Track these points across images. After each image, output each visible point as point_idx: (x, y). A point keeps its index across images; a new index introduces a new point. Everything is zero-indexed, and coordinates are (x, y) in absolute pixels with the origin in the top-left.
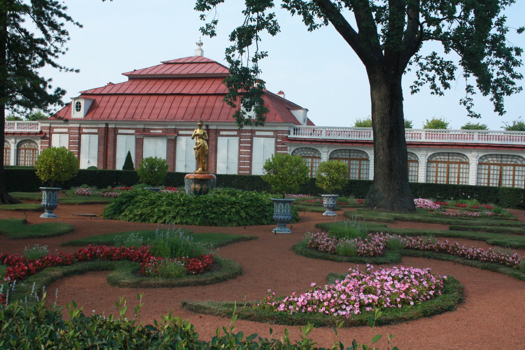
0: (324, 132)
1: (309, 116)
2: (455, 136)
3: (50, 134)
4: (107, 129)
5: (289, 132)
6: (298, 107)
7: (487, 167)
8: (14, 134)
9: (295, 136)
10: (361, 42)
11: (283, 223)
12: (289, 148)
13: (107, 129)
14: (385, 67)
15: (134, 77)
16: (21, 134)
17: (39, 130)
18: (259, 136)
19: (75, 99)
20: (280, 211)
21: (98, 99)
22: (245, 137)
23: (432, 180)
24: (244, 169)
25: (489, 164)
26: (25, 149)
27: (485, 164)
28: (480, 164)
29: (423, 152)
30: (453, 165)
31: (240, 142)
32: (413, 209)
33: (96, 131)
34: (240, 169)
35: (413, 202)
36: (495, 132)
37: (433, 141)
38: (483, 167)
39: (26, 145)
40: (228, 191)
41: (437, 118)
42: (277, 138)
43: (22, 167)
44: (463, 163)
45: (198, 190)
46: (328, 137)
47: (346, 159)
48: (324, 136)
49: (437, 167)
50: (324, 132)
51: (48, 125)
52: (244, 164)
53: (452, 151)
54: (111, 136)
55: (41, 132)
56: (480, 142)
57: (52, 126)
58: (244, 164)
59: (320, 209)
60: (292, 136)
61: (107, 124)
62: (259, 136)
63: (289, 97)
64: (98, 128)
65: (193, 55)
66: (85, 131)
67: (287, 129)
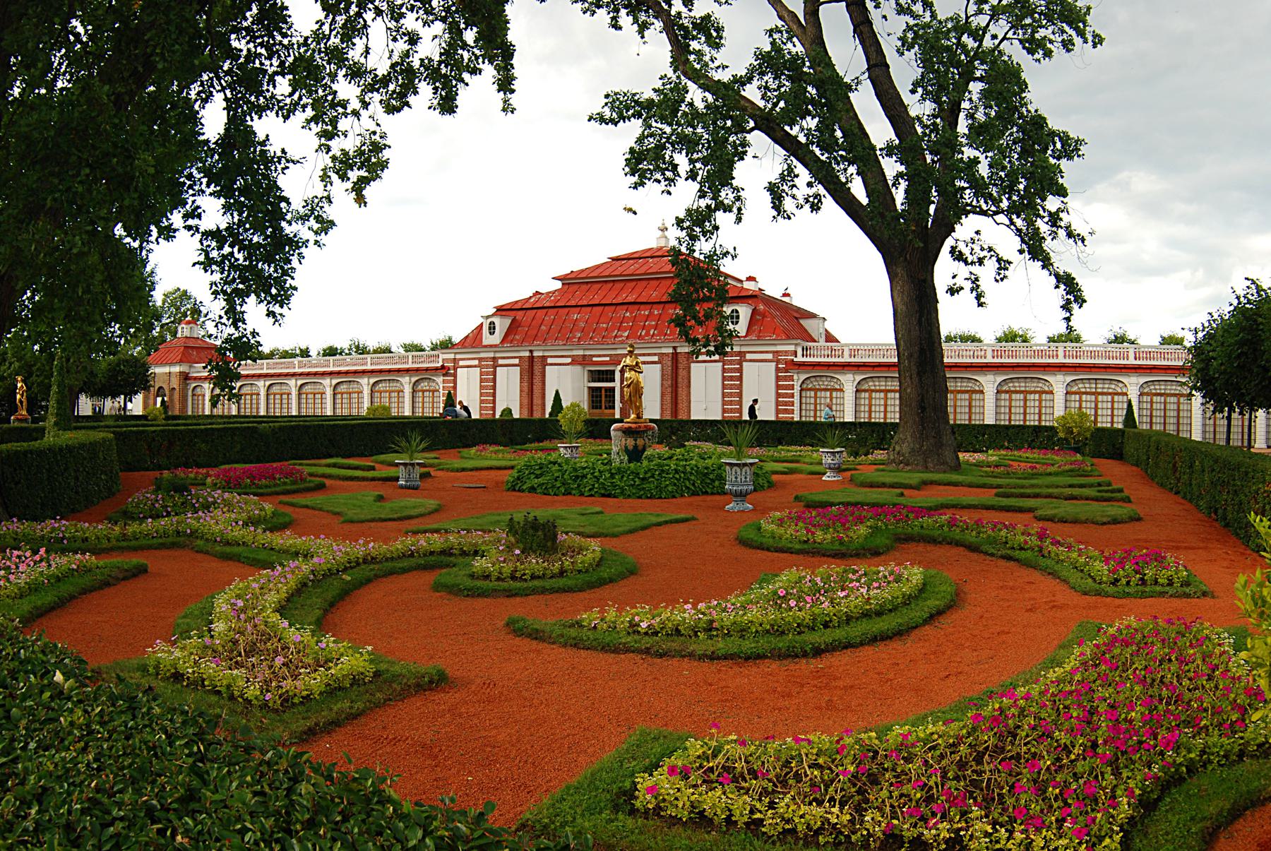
0: (846, 353)
1: (828, 325)
2: (1092, 354)
3: (455, 369)
4: (532, 358)
5: (795, 354)
6: (812, 316)
7: (1077, 397)
8: (408, 370)
9: (805, 359)
10: (874, 219)
11: (741, 495)
12: (795, 377)
13: (532, 358)
14: (909, 250)
15: (569, 281)
16: (417, 370)
17: (439, 365)
18: (751, 361)
19: (488, 317)
20: (736, 480)
21: (520, 315)
22: (731, 362)
23: (864, 418)
24: (731, 411)
25: (1081, 393)
26: (423, 391)
27: (1075, 393)
28: (1141, 394)
29: (990, 377)
30: (1032, 396)
31: (724, 370)
32: (957, 467)
33: (516, 361)
34: (724, 411)
35: (958, 458)
36: (1093, 346)
37: (1003, 361)
38: (1003, 396)
39: (424, 385)
40: (563, 450)
41: (1016, 327)
42: (778, 362)
43: (395, 418)
44: (836, 390)
45: (631, 448)
46: (852, 360)
47: (880, 391)
48: (847, 359)
49: (870, 398)
50: (846, 353)
51: (452, 356)
52: (731, 403)
53: (1023, 371)
54: (537, 368)
55: (443, 367)
56: (1067, 361)
57: (458, 356)
58: (731, 403)
59: (817, 468)
60: (799, 359)
61: (531, 351)
62: (751, 361)
63: (798, 301)
64: (520, 358)
65: (654, 245)
66: (501, 362)
67: (792, 348)
